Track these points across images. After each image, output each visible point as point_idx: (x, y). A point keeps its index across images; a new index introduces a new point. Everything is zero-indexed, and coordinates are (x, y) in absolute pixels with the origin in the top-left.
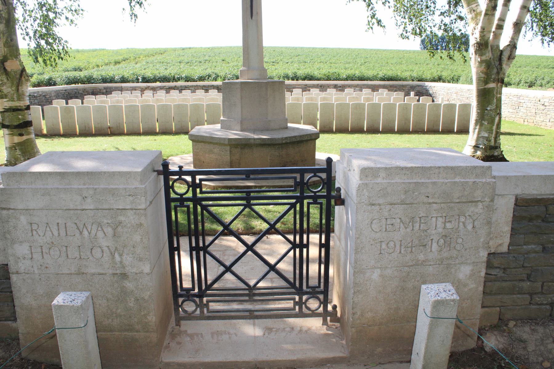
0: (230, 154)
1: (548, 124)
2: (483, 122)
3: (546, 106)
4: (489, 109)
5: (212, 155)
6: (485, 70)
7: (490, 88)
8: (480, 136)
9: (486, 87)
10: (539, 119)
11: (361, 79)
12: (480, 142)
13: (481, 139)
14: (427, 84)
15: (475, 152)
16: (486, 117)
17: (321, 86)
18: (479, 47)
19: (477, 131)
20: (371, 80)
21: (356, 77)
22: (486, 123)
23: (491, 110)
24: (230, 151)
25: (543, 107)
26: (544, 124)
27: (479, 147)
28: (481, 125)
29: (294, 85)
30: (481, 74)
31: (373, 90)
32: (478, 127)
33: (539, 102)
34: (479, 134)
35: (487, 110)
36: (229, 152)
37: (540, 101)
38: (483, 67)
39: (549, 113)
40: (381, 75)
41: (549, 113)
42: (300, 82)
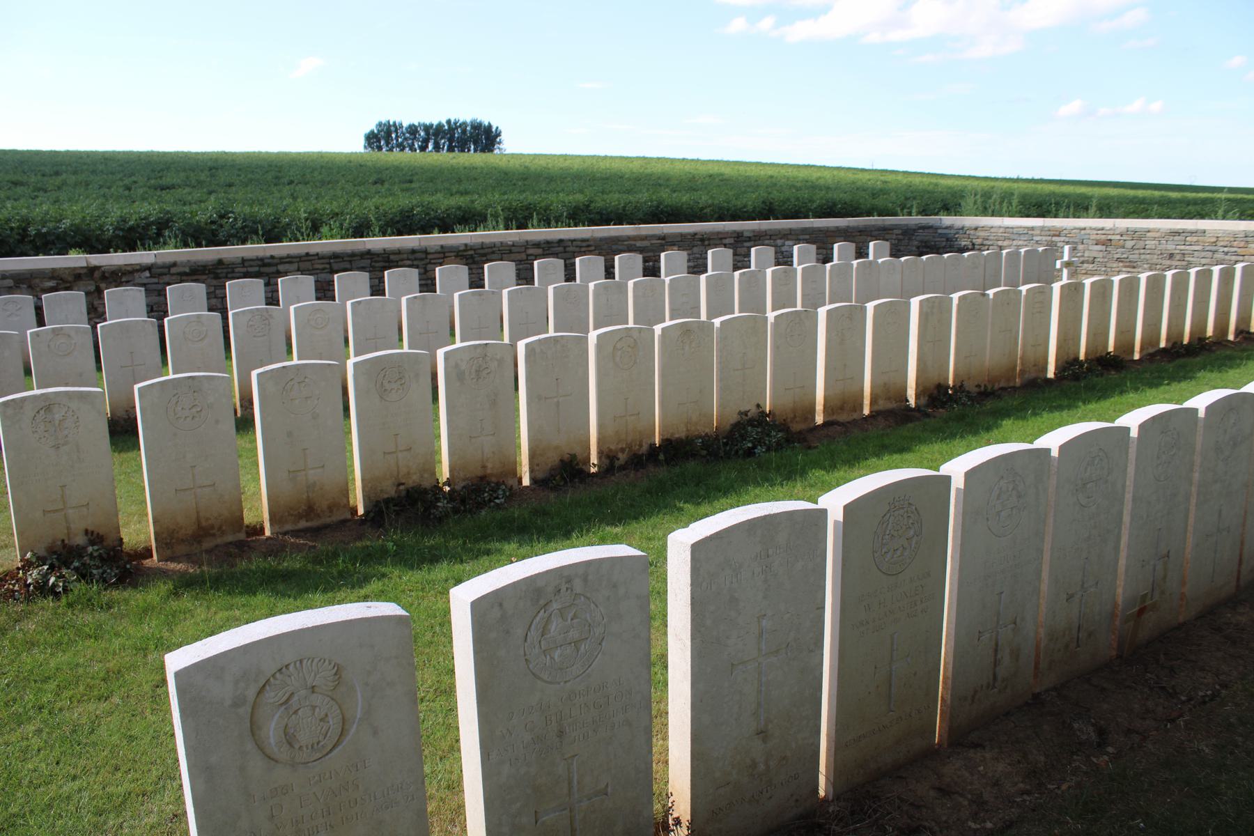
17: (597, 247)
29: (629, 238)
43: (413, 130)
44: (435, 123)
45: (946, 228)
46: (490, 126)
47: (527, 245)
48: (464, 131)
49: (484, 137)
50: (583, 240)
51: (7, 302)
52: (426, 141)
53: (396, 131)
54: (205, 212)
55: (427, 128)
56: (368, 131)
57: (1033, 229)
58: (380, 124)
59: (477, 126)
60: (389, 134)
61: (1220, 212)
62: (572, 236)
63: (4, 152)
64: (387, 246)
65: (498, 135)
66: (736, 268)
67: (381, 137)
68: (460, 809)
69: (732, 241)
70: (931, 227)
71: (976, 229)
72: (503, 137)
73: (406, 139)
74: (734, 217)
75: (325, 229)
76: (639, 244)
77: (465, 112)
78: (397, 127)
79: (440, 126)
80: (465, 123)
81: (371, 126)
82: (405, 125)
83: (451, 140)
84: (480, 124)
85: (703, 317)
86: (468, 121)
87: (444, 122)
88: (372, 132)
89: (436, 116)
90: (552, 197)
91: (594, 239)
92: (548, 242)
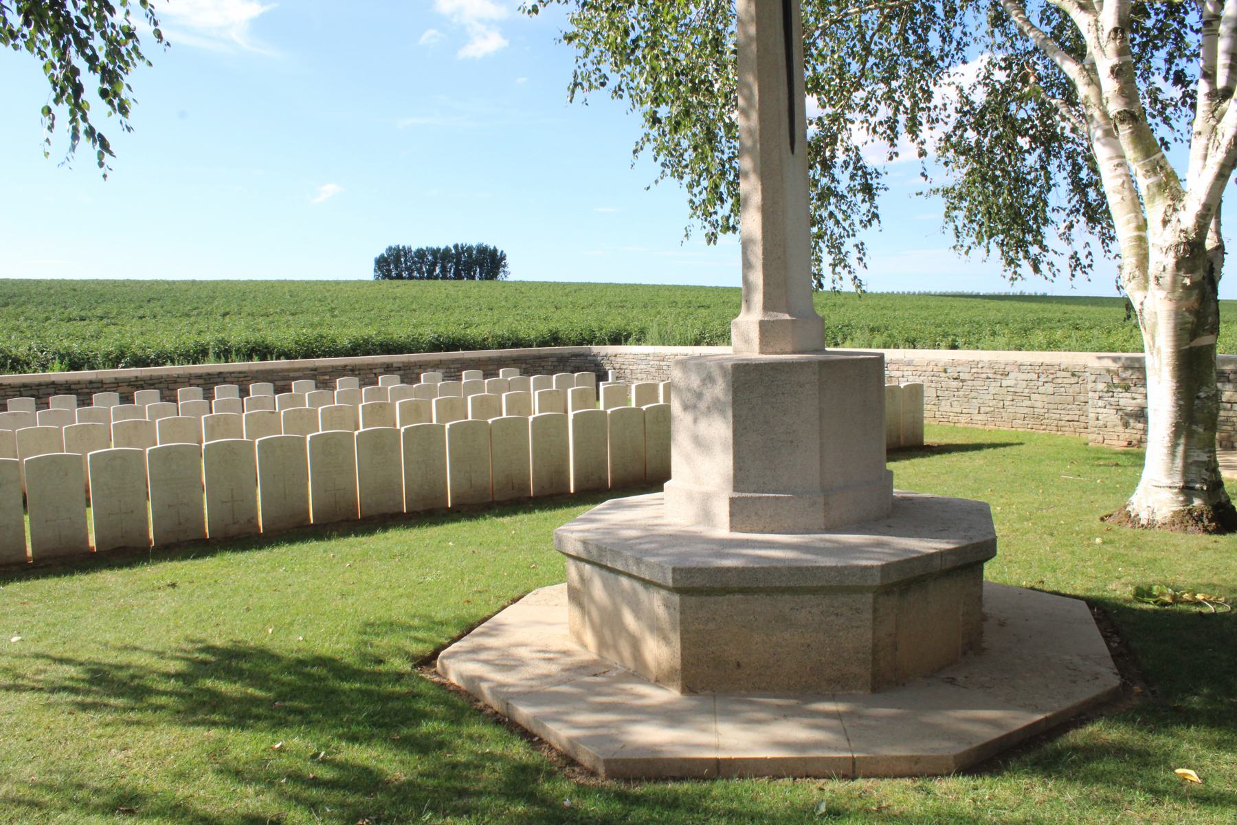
0: (874, 619)
1: (977, 417)
2: (1194, 427)
3: (963, 381)
4: (1202, 395)
5: (787, 635)
6: (1196, 306)
7: (1202, 347)
8: (1190, 461)
9: (1193, 344)
10: (948, 408)
11: (453, 345)
12: (1193, 476)
13: (1194, 469)
14: (595, 349)
15: (1188, 501)
16: (1198, 415)
17: (353, 370)
18: (1192, 252)
19: (1180, 449)
20: (411, 352)
21: (373, 344)
22: (1201, 430)
23: (1207, 398)
24: (875, 610)
25: (955, 384)
26: (963, 419)
27: (1193, 488)
28: (1190, 435)
29: (283, 370)
30: (1187, 314)
31: (527, 372)
32: (1182, 441)
33: (943, 375)
34: (1186, 456)
35: (1198, 398)
36: (868, 615)
37: (945, 371)
38: (1194, 298)
39: (973, 394)
40: (429, 333)
41: (973, 394)
42: (237, 365)
43: (421, 254)
44: (442, 247)
46: (495, 250)
47: (454, 361)
48: (470, 255)
49: (487, 263)
50: (240, 373)
52: (434, 265)
53: (405, 255)
54: (238, 334)
55: (434, 252)
57: (648, 355)
58: (390, 249)
59: (483, 250)
60: (398, 257)
62: (232, 370)
63: (4, 282)
64: (68, 378)
65: (503, 258)
66: (38, 409)
67: (393, 264)
72: (508, 260)
73: (414, 263)
74: (389, 352)
77: (472, 237)
78: (406, 252)
79: (447, 250)
80: (470, 249)
81: (381, 250)
82: (414, 249)
83: (457, 264)
84: (486, 249)
85: (434, 422)
86: (474, 245)
87: (451, 246)
88: (382, 256)
89: (443, 239)
90: (325, 331)
91: (252, 372)
92: (209, 374)
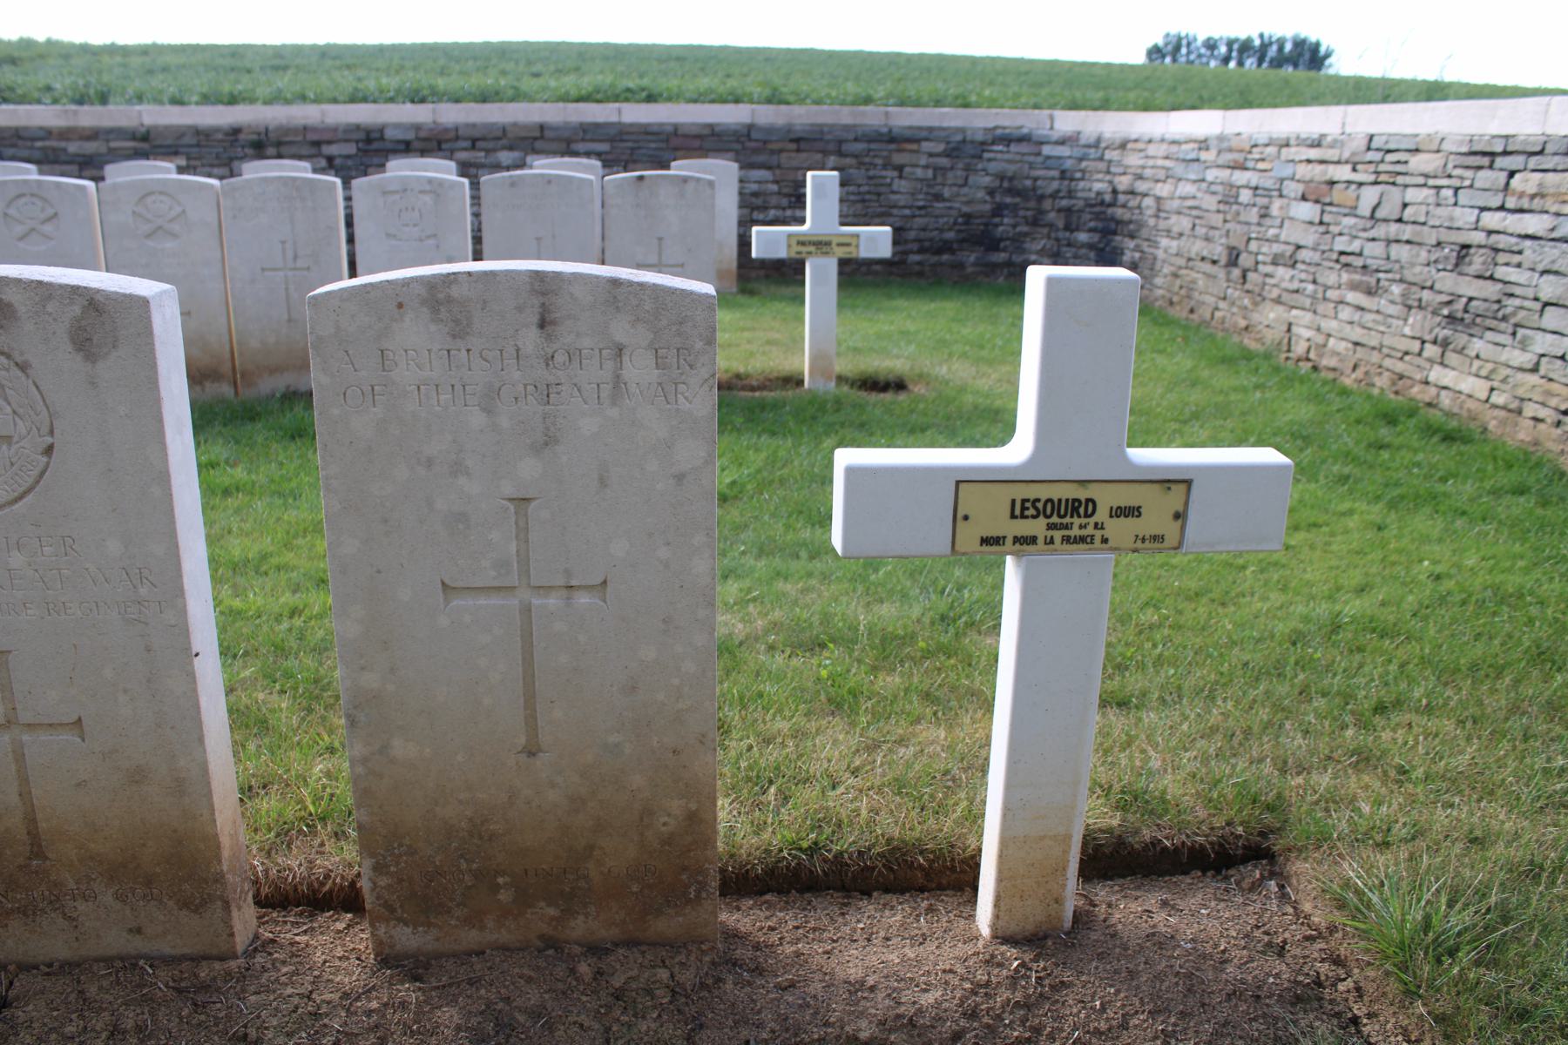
29: (48, 133)
45: (1062, 142)
46: (1318, 45)
48: (1281, 49)
51: (25, 192)
53: (1189, 44)
56: (1150, 45)
59: (1299, 44)
60: (1177, 48)
61: (1252, 440)
65: (1328, 55)
68: (1239, 442)
69: (351, 149)
70: (1024, 139)
71: (1123, 146)
75: (111, 99)
76: (73, 147)
77: (1284, 26)
82: (1201, 39)
84: (1304, 42)
